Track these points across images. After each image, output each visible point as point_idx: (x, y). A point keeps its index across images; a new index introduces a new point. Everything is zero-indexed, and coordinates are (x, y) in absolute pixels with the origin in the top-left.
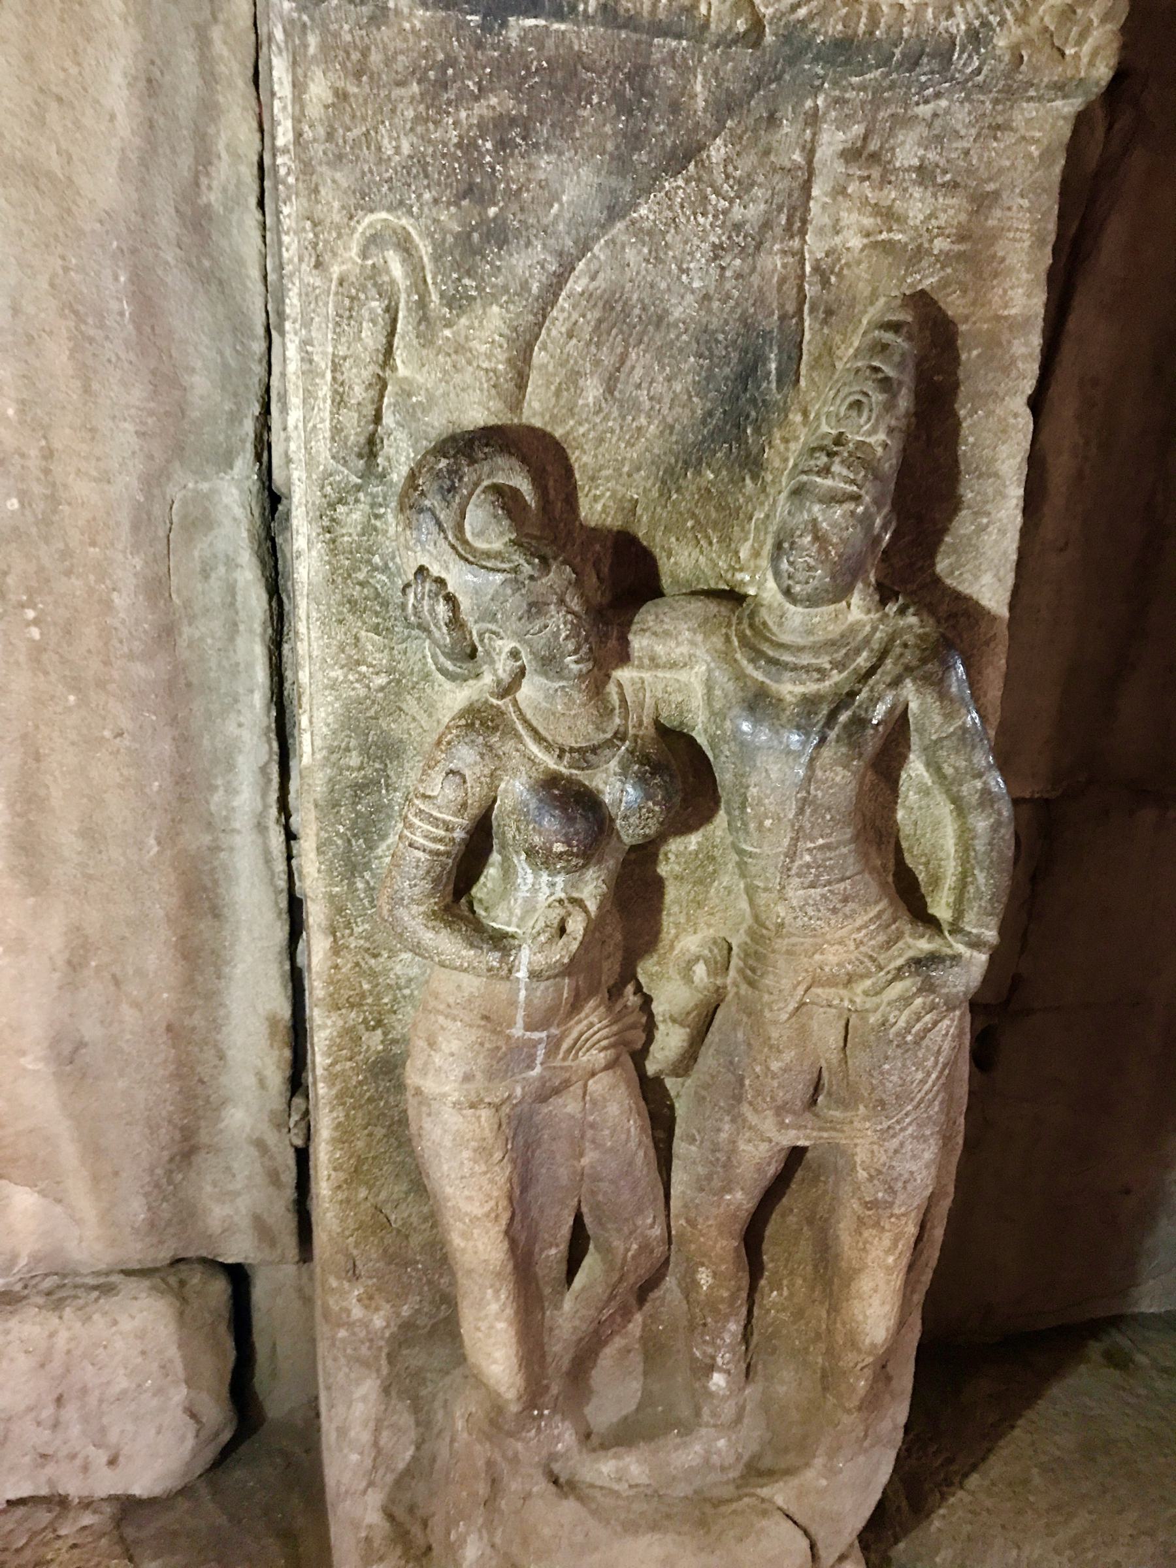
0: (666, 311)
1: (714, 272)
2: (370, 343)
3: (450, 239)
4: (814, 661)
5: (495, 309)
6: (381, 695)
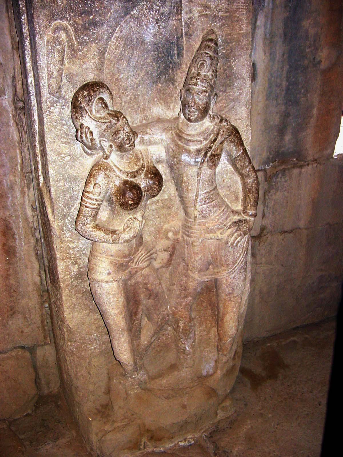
0: (144, 40)
1: (157, 27)
2: (57, 58)
3: (79, 26)
4: (198, 139)
5: (94, 45)
6: (69, 163)
